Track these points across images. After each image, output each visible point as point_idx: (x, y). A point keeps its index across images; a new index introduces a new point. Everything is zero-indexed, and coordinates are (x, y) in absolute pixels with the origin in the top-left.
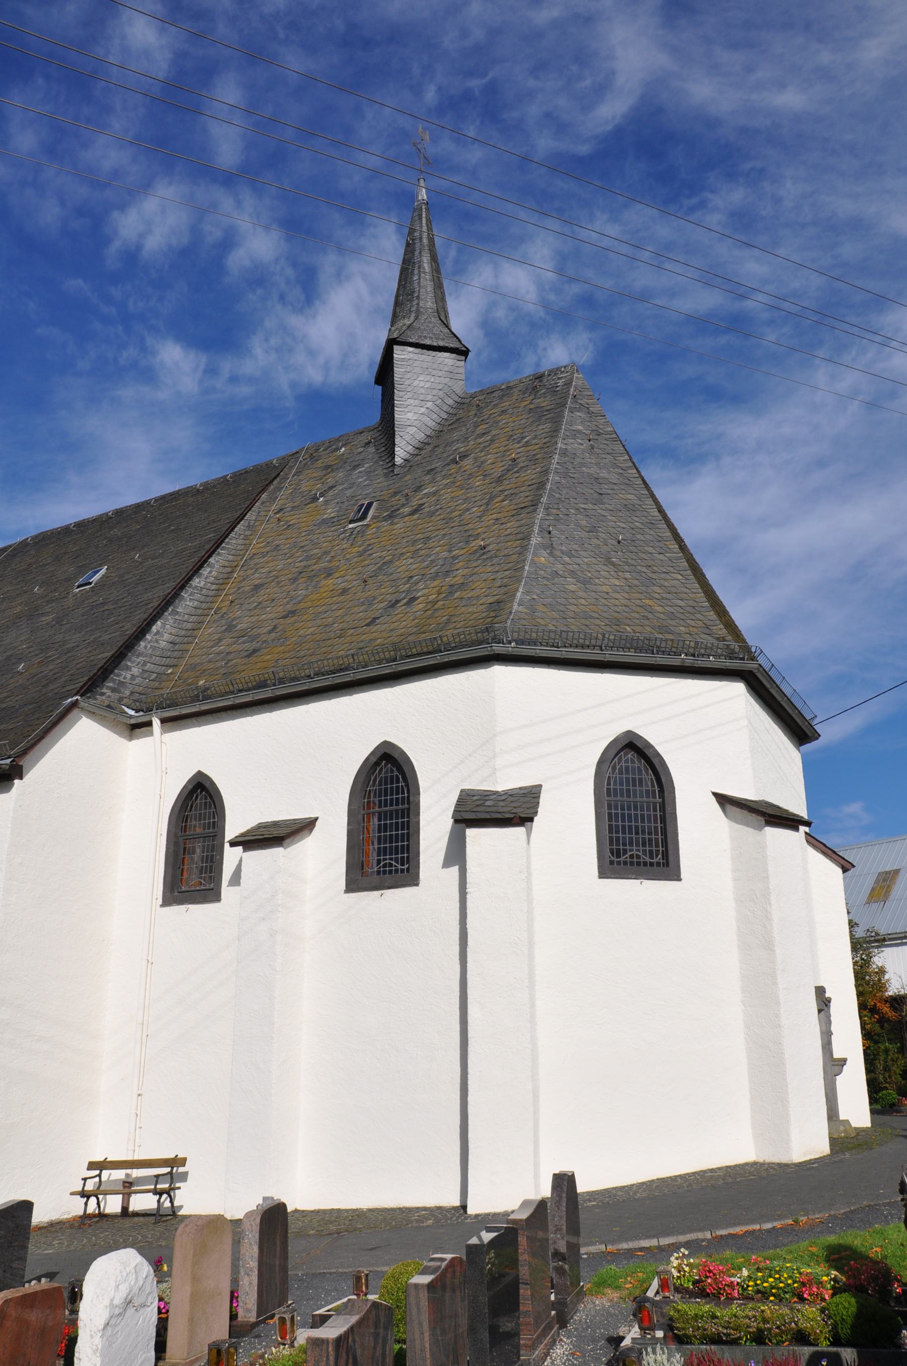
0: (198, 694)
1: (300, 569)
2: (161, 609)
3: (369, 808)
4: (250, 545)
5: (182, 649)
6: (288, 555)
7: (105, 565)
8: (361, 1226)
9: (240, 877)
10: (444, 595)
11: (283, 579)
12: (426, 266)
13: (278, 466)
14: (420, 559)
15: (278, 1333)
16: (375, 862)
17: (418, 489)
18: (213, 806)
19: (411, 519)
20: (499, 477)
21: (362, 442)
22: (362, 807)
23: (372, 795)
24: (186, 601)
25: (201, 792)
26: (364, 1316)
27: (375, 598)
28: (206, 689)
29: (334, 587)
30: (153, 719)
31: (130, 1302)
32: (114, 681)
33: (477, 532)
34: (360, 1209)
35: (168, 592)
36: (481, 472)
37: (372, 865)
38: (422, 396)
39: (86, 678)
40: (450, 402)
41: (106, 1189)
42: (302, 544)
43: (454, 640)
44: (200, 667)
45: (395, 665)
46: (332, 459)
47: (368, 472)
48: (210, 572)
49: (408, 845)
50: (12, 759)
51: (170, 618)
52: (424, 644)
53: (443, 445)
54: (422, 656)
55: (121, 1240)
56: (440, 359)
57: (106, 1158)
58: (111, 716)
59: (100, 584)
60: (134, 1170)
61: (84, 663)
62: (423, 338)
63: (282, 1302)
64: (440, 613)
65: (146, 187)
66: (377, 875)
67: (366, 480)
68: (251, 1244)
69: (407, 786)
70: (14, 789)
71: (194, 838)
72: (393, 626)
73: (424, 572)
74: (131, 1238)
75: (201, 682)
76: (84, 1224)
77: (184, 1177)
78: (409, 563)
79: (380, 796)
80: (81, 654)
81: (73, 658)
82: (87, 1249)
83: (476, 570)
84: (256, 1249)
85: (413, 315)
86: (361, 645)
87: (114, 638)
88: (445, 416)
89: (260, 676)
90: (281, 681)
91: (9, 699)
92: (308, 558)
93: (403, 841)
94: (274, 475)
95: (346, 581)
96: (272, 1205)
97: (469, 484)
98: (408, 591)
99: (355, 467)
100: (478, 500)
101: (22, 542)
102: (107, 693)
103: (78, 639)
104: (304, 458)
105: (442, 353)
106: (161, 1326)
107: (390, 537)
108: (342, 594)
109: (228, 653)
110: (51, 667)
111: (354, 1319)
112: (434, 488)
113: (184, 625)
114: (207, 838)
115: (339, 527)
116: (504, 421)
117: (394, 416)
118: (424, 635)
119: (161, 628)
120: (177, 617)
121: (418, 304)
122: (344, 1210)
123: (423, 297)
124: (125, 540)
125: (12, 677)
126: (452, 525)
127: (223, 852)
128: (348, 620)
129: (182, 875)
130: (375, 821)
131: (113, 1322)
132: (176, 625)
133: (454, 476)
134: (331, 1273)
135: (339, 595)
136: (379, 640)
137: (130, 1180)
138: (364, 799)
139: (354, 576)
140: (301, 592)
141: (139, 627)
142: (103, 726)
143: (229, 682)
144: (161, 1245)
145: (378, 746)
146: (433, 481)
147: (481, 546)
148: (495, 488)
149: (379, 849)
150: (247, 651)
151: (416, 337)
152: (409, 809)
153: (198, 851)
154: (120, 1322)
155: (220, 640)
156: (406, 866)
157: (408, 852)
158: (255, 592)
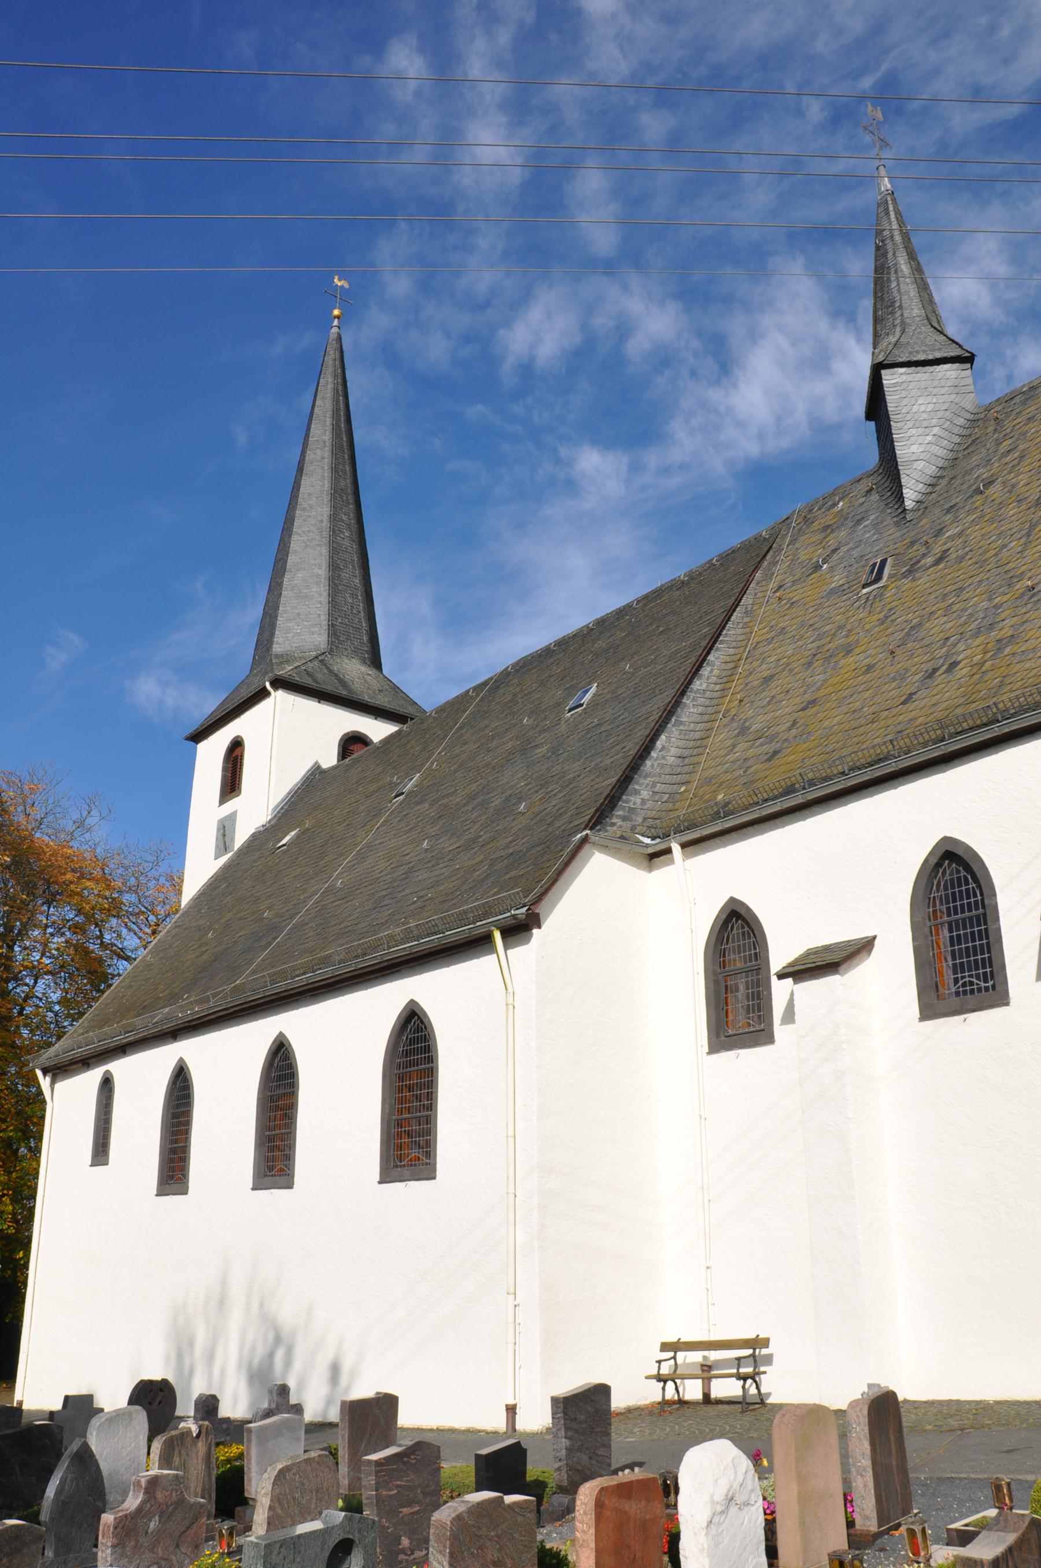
0: (718, 810)
1: (813, 651)
2: (663, 721)
3: (936, 918)
4: (752, 633)
5: (692, 762)
6: (797, 637)
7: (594, 683)
8: (990, 1422)
9: (794, 1014)
10: (992, 653)
11: (795, 666)
12: (905, 268)
13: (770, 537)
14: (955, 615)
15: (908, 1547)
16: (952, 981)
17: (939, 532)
18: (752, 935)
19: (937, 570)
20: (1038, 498)
21: (862, 491)
22: (927, 918)
23: (938, 902)
24: (689, 708)
25: (737, 921)
26: (1023, 1535)
27: (907, 670)
28: (727, 804)
29: (858, 664)
30: (672, 845)
31: (732, 1498)
32: (623, 808)
33: (1020, 572)
34: (985, 1401)
35: (668, 701)
36: (1013, 498)
37: (948, 986)
38: (924, 422)
39: (593, 810)
40: (961, 421)
41: (684, 1373)
42: (811, 622)
43: (1012, 705)
44: (717, 780)
45: (944, 745)
46: (830, 517)
47: (875, 525)
48: (711, 671)
49: (990, 958)
50: (527, 907)
51: (674, 729)
52: (976, 715)
53: (960, 476)
54: (976, 730)
55: (707, 1430)
56: (940, 374)
57: (680, 1339)
59: (592, 704)
61: (589, 793)
62: (914, 354)
63: (906, 1511)
64: (989, 675)
65: (523, 300)
66: (956, 997)
67: (874, 534)
68: (860, 1439)
69: (979, 887)
70: (534, 940)
71: (736, 973)
72: (934, 700)
73: (962, 630)
74: (718, 1428)
75: (720, 797)
76: (664, 1412)
77: (768, 1360)
78: (942, 622)
79: (948, 903)
80: (584, 784)
82: (671, 1439)
83: (1028, 615)
84: (866, 1445)
85: (898, 329)
86: (899, 728)
87: (617, 761)
88: (957, 440)
89: (786, 780)
90: (812, 783)
91: (515, 843)
92: (820, 637)
93: (983, 953)
94: (766, 549)
95: (870, 656)
96: (879, 1394)
97: (1001, 515)
98: (947, 656)
99: (859, 522)
100: (1015, 533)
101: (503, 672)
102: (617, 821)
103: (578, 767)
104: (797, 522)
105: (942, 366)
106: (767, 1529)
107: (915, 596)
108: (867, 672)
109: (745, 759)
110: (554, 802)
111: (1011, 1538)
112: (959, 528)
113: (691, 735)
114: (750, 973)
115: (851, 594)
116: (1033, 431)
117: (895, 453)
118: (974, 705)
119: (666, 743)
121: (902, 315)
122: (964, 1401)
123: (906, 305)
124: (612, 650)
125: (514, 819)
126: (988, 568)
127: (770, 987)
128: (879, 701)
129: (727, 1017)
130: (945, 933)
131: (716, 1520)
132: (682, 736)
133: (981, 508)
134: (961, 1479)
135: (863, 674)
136: (920, 719)
137: (709, 1363)
138: (929, 908)
139: (878, 648)
140: (818, 677)
143: (752, 793)
144: (752, 1437)
145: (937, 844)
146: (956, 520)
147: (1028, 586)
148: (1034, 513)
149: (954, 965)
150: (766, 754)
151: (907, 355)
152: (985, 915)
153: (742, 988)
154: (724, 1521)
155: (734, 746)
156: (991, 983)
157: (991, 966)
158: (765, 686)
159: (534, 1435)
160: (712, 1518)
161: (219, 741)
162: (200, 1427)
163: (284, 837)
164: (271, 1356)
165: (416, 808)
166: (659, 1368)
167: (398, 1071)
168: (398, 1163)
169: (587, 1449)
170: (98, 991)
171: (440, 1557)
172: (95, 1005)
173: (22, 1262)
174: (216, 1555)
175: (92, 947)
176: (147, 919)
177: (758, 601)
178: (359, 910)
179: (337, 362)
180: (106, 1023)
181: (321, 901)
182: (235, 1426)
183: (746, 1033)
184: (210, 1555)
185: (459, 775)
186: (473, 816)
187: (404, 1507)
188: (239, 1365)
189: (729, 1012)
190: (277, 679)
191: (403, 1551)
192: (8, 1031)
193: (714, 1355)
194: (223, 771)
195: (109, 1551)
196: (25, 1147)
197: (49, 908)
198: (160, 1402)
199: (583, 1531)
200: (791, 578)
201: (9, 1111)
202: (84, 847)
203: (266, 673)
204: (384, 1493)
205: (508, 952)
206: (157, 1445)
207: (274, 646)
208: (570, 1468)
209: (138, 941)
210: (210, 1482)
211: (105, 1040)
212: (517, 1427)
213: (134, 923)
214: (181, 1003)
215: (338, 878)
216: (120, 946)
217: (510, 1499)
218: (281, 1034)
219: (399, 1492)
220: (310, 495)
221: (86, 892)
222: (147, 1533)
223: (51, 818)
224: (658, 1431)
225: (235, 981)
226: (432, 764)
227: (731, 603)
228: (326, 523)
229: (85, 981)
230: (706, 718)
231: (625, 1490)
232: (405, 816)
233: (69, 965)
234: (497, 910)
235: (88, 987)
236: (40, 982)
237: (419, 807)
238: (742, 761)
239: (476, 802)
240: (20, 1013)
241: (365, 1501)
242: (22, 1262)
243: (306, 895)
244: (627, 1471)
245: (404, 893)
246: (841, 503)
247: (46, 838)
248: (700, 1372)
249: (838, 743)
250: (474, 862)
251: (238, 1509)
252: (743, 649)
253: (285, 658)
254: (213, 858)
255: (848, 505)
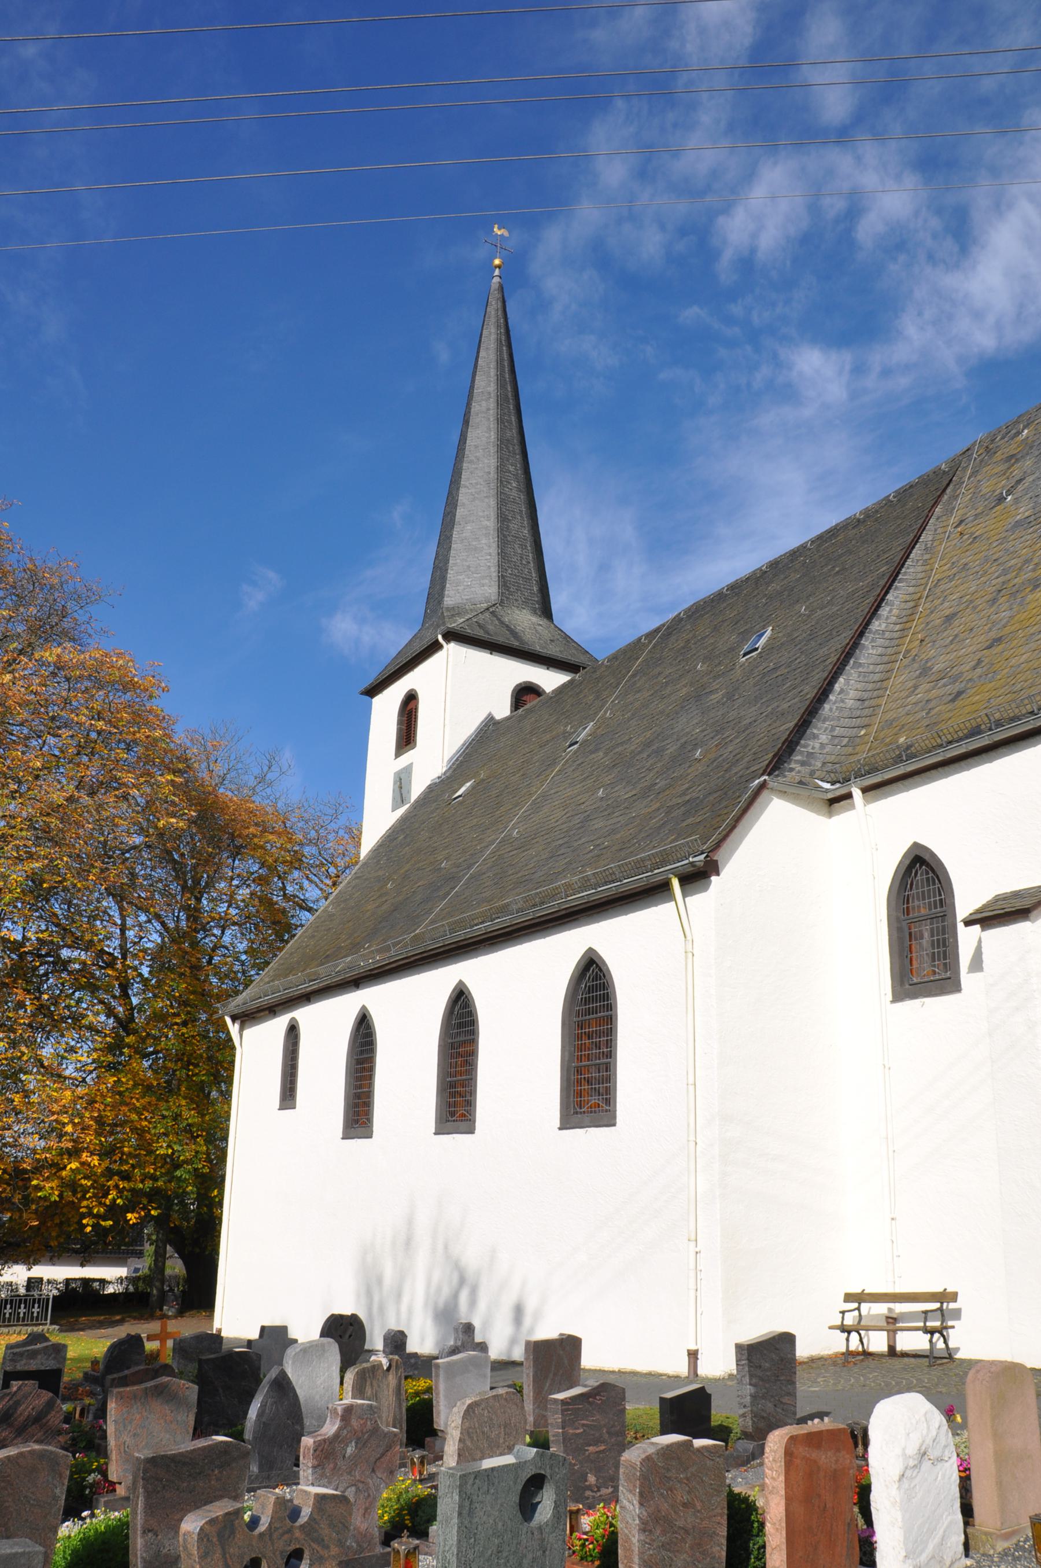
1: (998, 587)
4: (932, 570)
9: (982, 961)
13: (949, 471)
24: (868, 649)
25: (920, 867)
28: (909, 747)
31: (925, 1453)
39: (770, 755)
48: (890, 611)
55: (894, 1383)
58: (804, 793)
60: (897, 1305)
71: (920, 920)
75: (902, 740)
77: (957, 1314)
81: (751, 735)
87: (794, 705)
90: (999, 724)
92: (1005, 572)
102: (795, 766)
104: (979, 453)
109: (927, 701)
110: (730, 749)
113: (871, 677)
120: (861, 670)
124: (786, 593)
125: (690, 767)
127: (957, 934)
129: (911, 964)
131: (908, 1473)
132: (861, 679)
137: (895, 1316)
141: (820, 689)
142: (796, 805)
143: (935, 735)
144: (941, 1392)
153: (926, 935)
155: (916, 687)
158: (948, 624)
159: (716, 1381)
160: (904, 1472)
161: (395, 693)
162: (390, 1361)
163: (460, 788)
164: (456, 1296)
165: (591, 757)
166: (843, 1318)
167: (577, 1019)
168: (578, 1110)
169: (772, 1396)
170: (282, 941)
171: (630, 1496)
172: (280, 955)
173: (217, 1200)
174: (409, 1481)
175: (275, 898)
176: (327, 871)
177: (938, 537)
178: (535, 859)
179: (500, 313)
180: (291, 972)
181: (497, 851)
182: (422, 1361)
183: (931, 981)
184: (403, 1481)
185: (633, 722)
186: (648, 764)
187: (590, 1446)
188: (426, 1304)
189: (914, 959)
190: (448, 632)
191: (589, 1488)
192: (199, 980)
193: (900, 1308)
194: (398, 724)
195: (310, 1471)
196: (217, 1091)
197: (234, 861)
198: (350, 1336)
199: (773, 1478)
200: (973, 512)
201: (201, 1056)
202: (266, 802)
203: (438, 626)
204: (571, 1431)
205: (687, 899)
206: (350, 1376)
207: (445, 599)
208: (755, 1415)
209: (320, 892)
210: (401, 1413)
211: (290, 988)
212: (699, 1373)
213: (315, 875)
214: (363, 952)
215: (513, 828)
216: (302, 898)
217: (699, 1443)
218: (461, 983)
219: (584, 1431)
220: (476, 447)
221: (269, 846)
222: (344, 1457)
223: (233, 774)
224: (842, 1381)
225: (415, 930)
226: (606, 712)
227: (910, 540)
228: (493, 475)
229: (270, 932)
230: (886, 659)
231: (814, 1440)
232: (579, 765)
233: (254, 916)
234: (675, 857)
235: (273, 937)
236: (228, 932)
237: (593, 756)
238: (924, 702)
239: (650, 750)
240: (209, 962)
241: (551, 1438)
242: (217, 1200)
243: (483, 845)
244: (816, 1421)
245: (580, 842)
246: (1026, 431)
247: (229, 794)
248: (885, 1324)
249: (1026, 681)
250: (650, 810)
251: (428, 1439)
252: (923, 587)
253: (457, 611)
254: (390, 809)
255: (1034, 432)
